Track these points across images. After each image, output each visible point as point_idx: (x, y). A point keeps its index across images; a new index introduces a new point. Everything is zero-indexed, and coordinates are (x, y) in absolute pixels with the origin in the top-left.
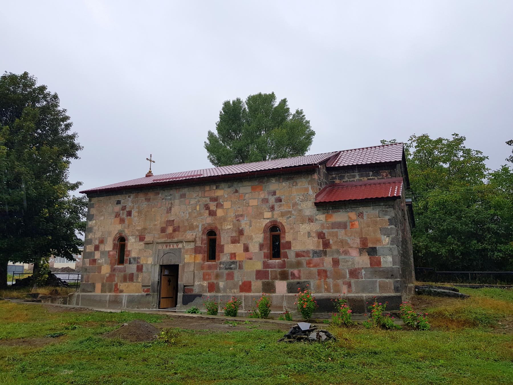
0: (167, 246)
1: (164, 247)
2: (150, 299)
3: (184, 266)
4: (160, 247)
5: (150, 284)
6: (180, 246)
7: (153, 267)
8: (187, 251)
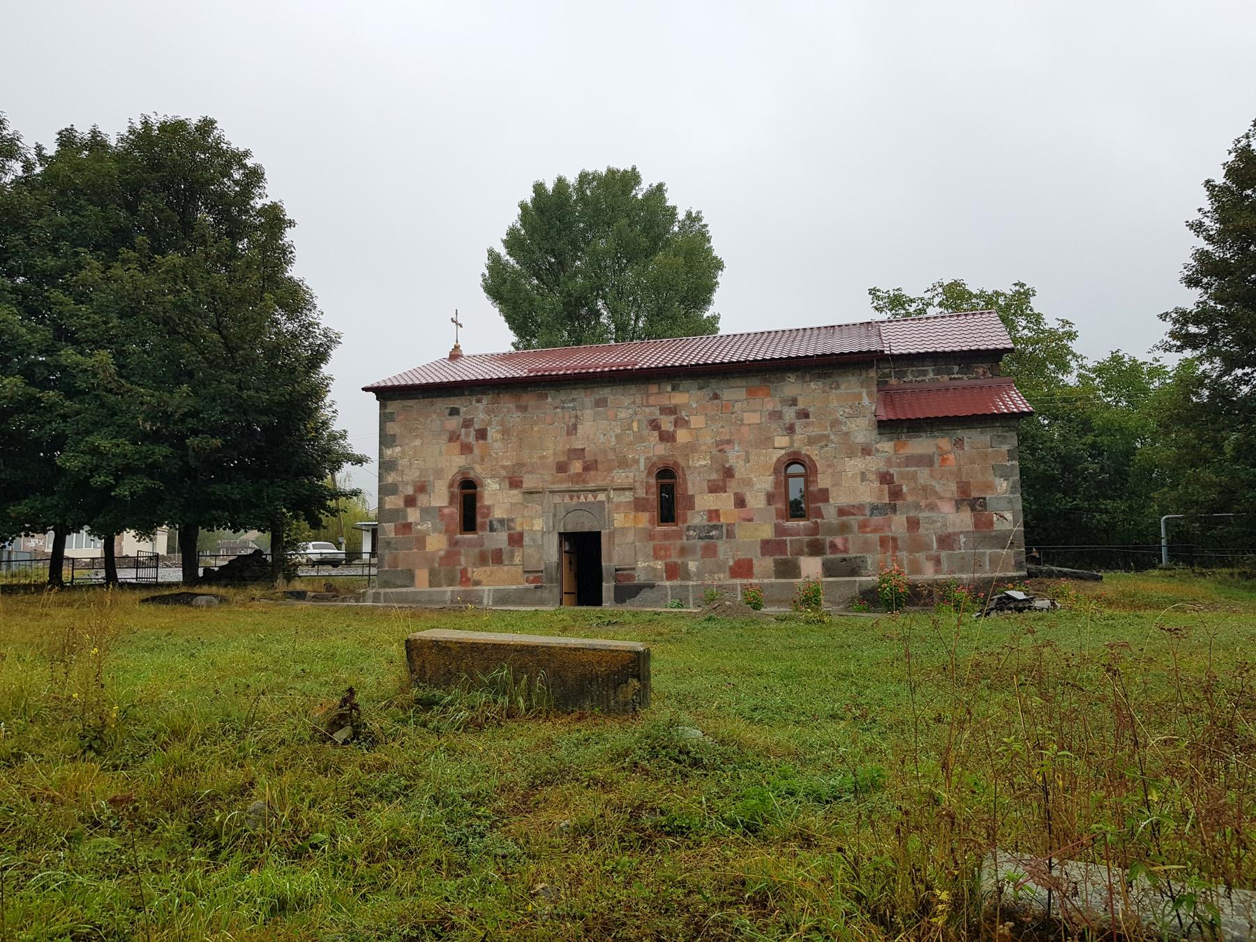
0: (571, 498)
1: (567, 499)
2: (546, 594)
3: (612, 535)
4: (557, 499)
5: (543, 568)
6: (601, 497)
7: (546, 538)
8: (618, 506)
